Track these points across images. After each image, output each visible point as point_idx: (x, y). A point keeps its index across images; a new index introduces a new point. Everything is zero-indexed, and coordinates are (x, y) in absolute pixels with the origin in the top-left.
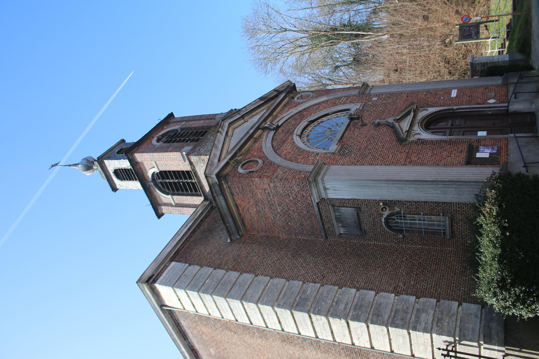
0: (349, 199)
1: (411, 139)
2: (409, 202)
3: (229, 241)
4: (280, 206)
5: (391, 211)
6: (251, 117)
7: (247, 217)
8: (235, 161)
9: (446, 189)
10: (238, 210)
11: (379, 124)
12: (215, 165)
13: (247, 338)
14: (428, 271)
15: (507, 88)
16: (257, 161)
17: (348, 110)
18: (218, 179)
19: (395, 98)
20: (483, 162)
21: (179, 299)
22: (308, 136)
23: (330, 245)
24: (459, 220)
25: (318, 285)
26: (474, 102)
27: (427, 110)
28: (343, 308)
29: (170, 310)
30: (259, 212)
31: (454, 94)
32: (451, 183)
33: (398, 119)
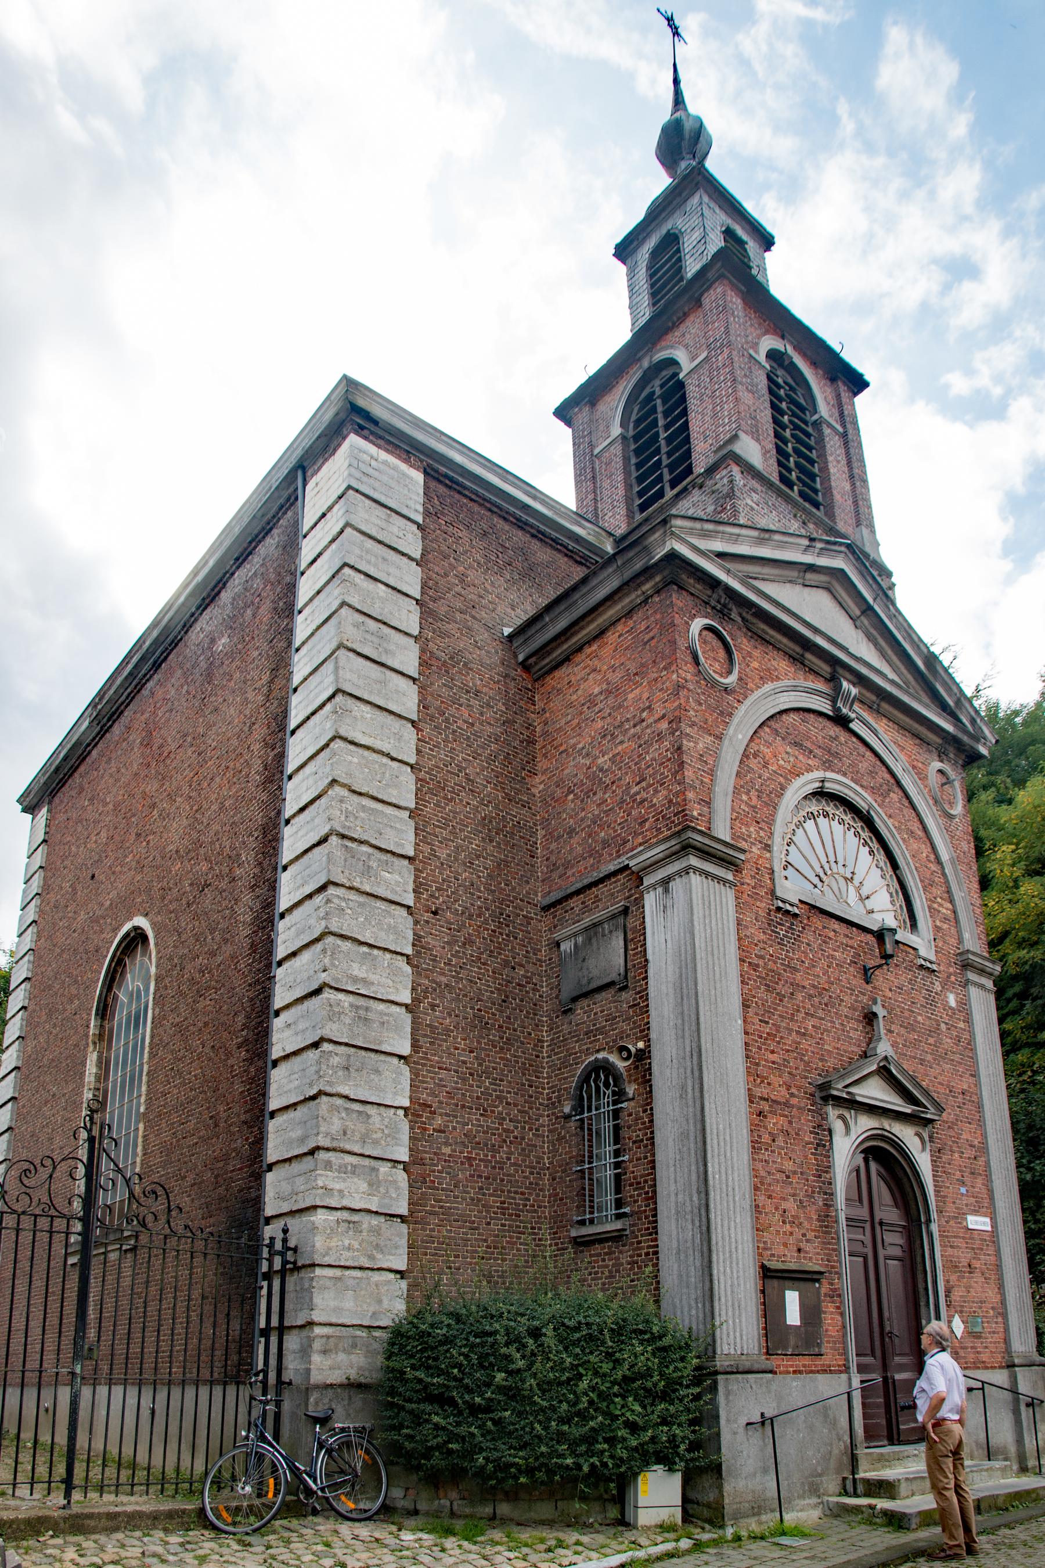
0: (645, 955)
1: (832, 1113)
2: (651, 1121)
3: (507, 631)
4: (612, 760)
5: (625, 1074)
6: (870, 638)
8: (724, 606)
9: (689, 1217)
10: (589, 642)
11: (870, 1018)
12: (703, 544)
13: (260, 732)
14: (481, 1188)
15: (1001, 1367)
16: (730, 672)
17: (914, 926)
18: (661, 560)
19: (957, 1057)
20: (771, 1312)
21: (324, 515)
22: (826, 815)
25: (409, 900)
26: (953, 1278)
27: (924, 1149)
28: (355, 973)
29: (296, 499)
30: (592, 702)
31: (978, 1222)
32: (704, 1228)
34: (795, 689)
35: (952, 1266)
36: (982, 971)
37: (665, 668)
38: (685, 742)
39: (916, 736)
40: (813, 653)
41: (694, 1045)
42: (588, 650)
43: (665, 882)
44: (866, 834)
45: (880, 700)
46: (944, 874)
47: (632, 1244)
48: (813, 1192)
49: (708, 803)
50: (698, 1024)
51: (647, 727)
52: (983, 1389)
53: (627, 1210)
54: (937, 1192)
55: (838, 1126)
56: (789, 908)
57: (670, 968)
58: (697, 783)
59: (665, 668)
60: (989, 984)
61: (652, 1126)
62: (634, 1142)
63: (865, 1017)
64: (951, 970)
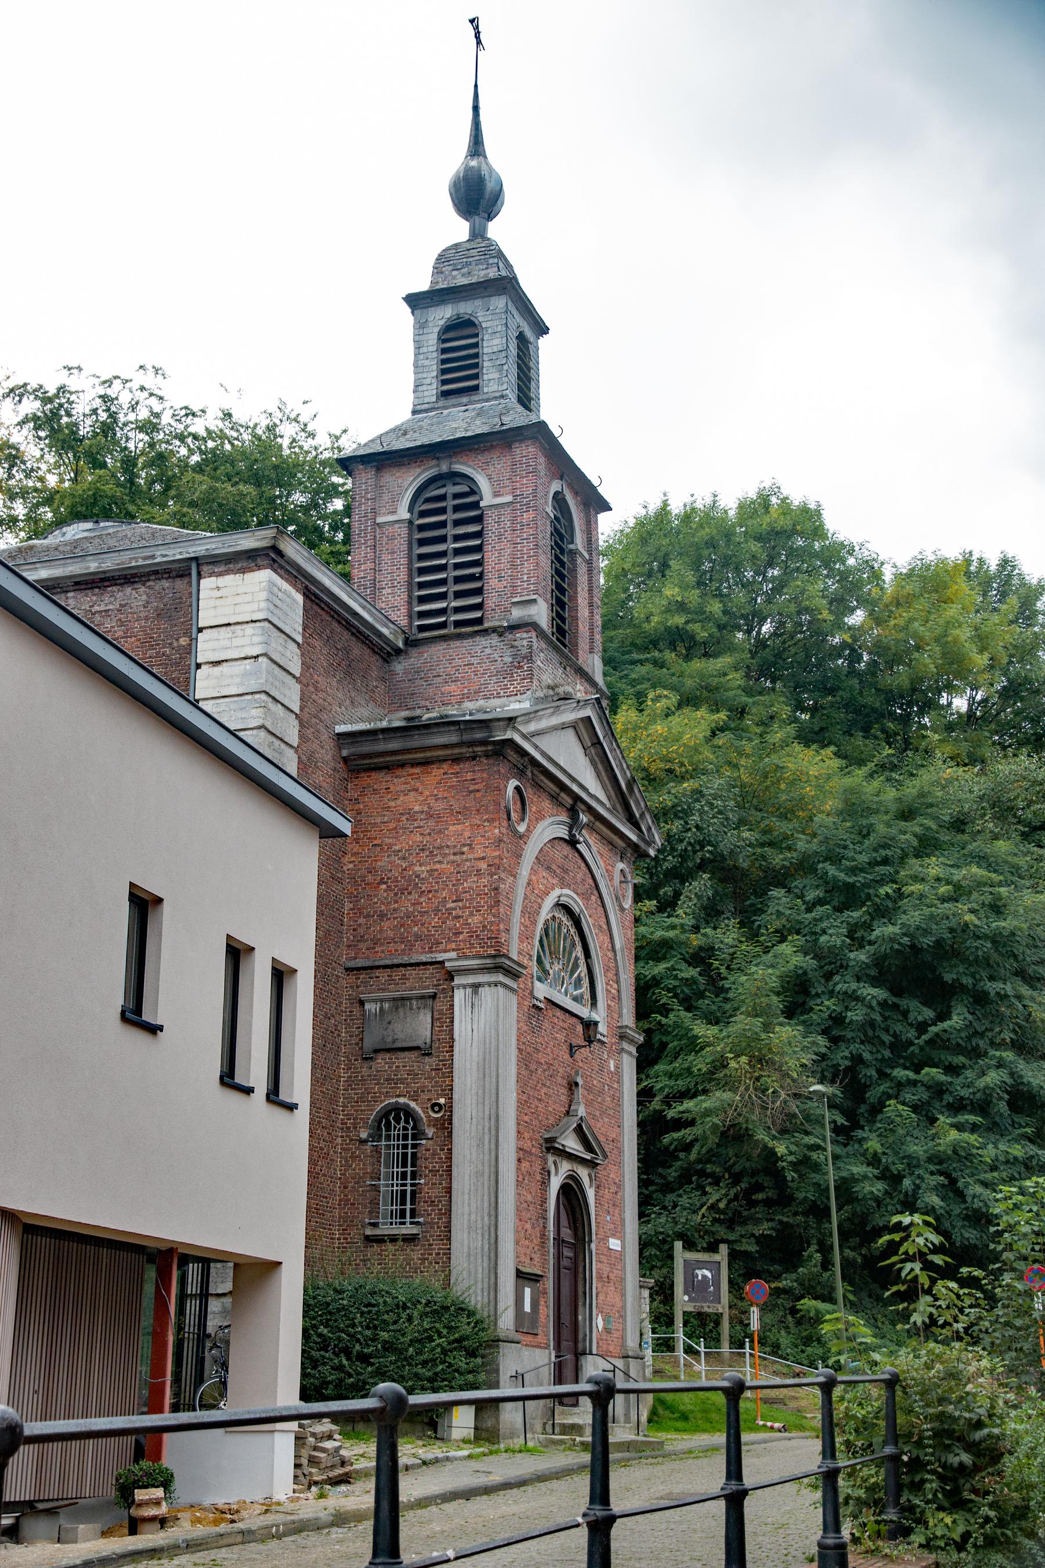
1: (551, 1159)
4: (431, 872)
7: (398, 782)
9: (479, 1231)
27: (591, 1186)
30: (412, 817)
31: (614, 1244)
32: (493, 1241)
36: (632, 1041)
39: (611, 843)
41: (493, 1112)
43: (476, 987)
46: (616, 960)
50: (497, 1097)
51: (467, 860)
53: (421, 1220)
55: (553, 1169)
57: (475, 1052)
60: (633, 1050)
62: (430, 1171)
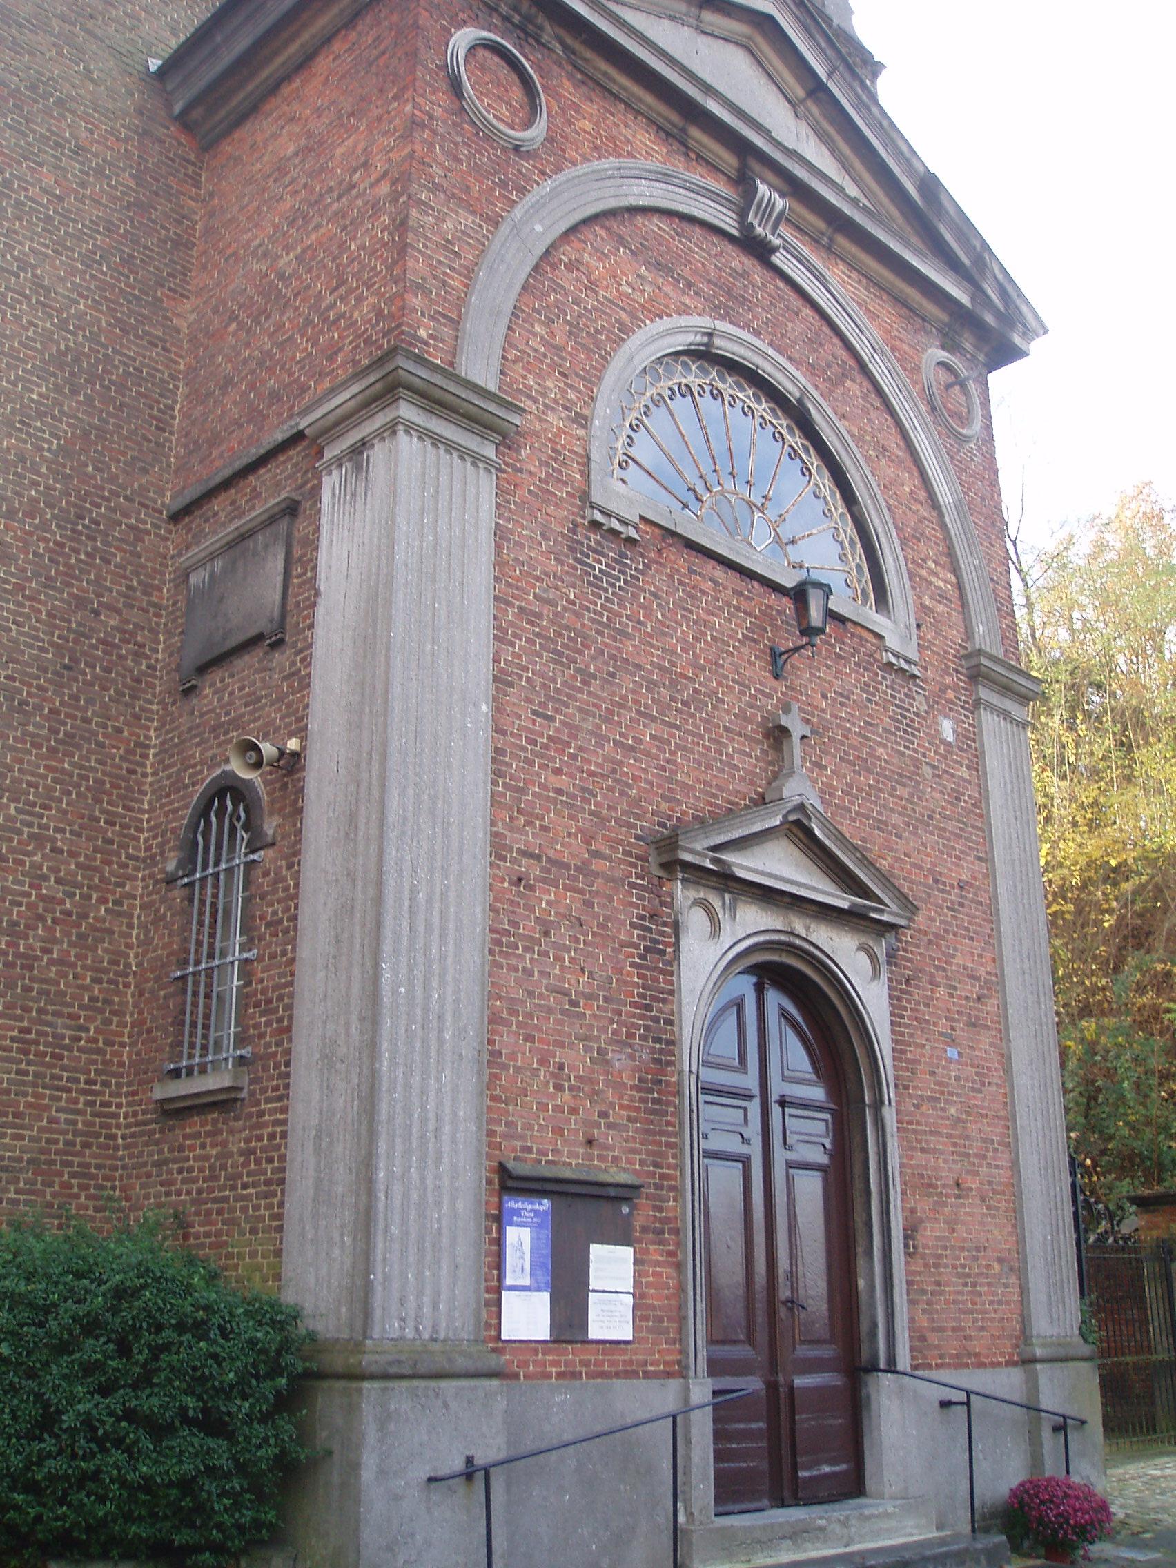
3: (154, 64)
6: (823, 137)
10: (287, 78)
16: (528, 124)
19: (951, 825)
22: (717, 395)
23: (138, 534)
24: (225, 1144)
26: (923, 1207)
27: (875, 976)
33: (809, 833)
34: (665, 178)
35: (922, 1184)
37: (395, 98)
38: (414, 212)
39: (900, 301)
40: (704, 129)
42: (286, 90)
44: (797, 440)
45: (835, 228)
46: (943, 526)
47: (250, 1115)
48: (630, 1035)
49: (456, 323)
52: (968, 1404)
54: (898, 1053)
55: (696, 920)
56: (615, 525)
58: (433, 285)
59: (395, 98)
61: (296, 896)
63: (767, 736)
64: (948, 680)
